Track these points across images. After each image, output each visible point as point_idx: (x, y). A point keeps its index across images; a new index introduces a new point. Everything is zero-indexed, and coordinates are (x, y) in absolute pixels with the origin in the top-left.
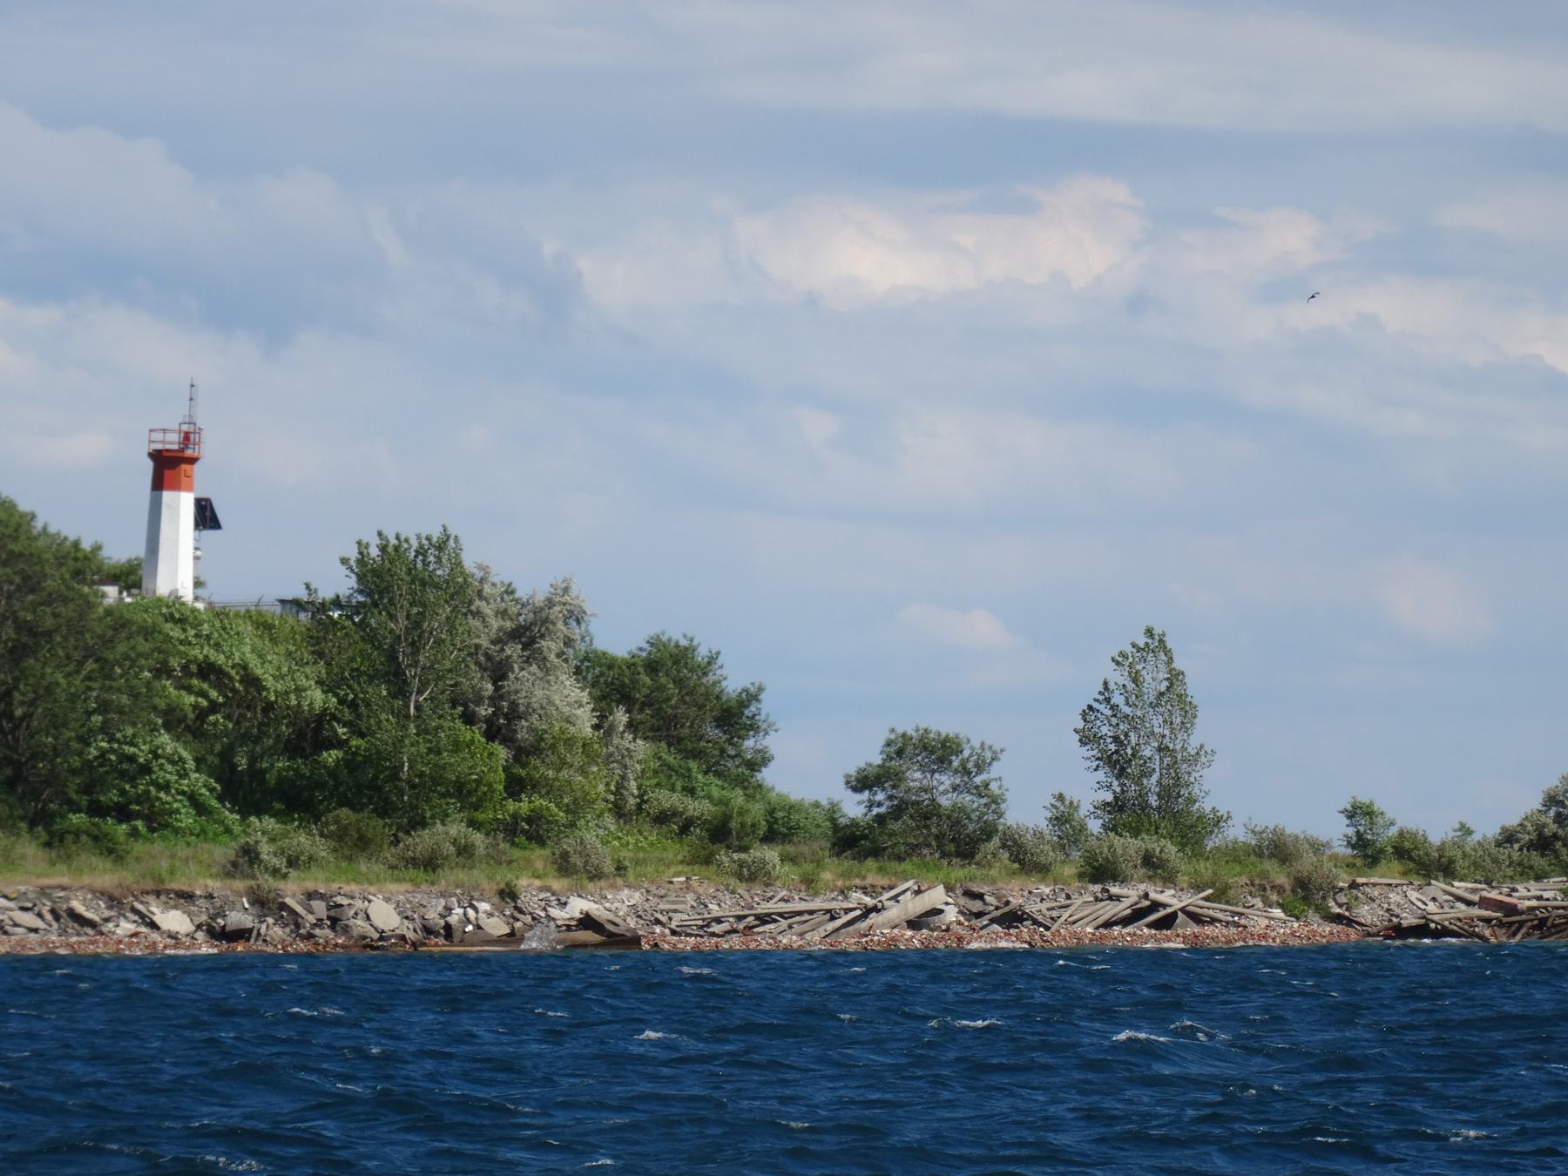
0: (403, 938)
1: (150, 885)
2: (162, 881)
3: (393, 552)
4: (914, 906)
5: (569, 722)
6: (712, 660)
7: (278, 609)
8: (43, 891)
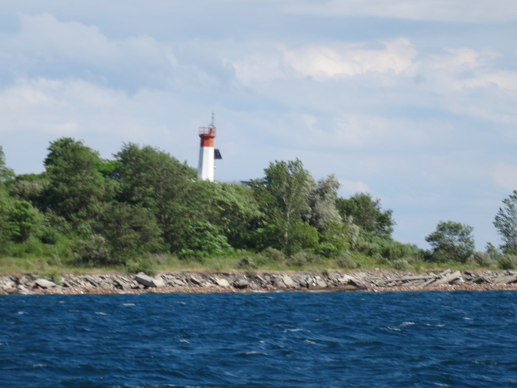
0: (294, 288)
1: (215, 271)
2: (219, 270)
3: (281, 166)
4: (451, 277)
5: (336, 219)
6: (378, 202)
7: (241, 184)
8: (183, 273)
